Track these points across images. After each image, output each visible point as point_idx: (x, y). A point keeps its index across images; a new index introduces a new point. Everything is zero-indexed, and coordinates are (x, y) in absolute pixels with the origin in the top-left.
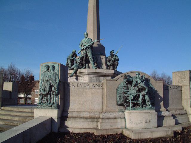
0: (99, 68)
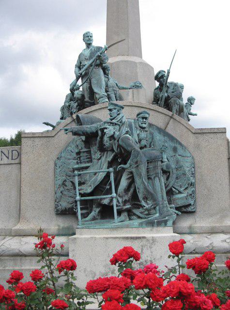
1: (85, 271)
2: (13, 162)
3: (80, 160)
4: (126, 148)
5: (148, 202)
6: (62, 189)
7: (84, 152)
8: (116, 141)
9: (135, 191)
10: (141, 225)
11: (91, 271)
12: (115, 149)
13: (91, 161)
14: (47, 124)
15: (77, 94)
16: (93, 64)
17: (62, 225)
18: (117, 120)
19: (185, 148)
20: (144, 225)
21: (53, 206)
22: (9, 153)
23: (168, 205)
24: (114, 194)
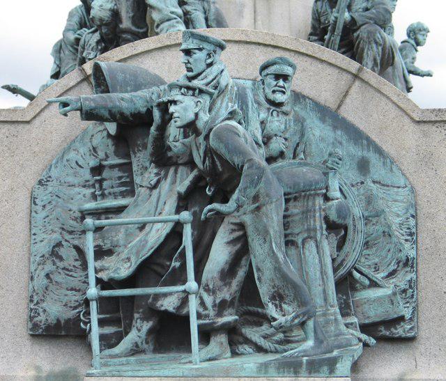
4: (227, 157)
5: (283, 305)
6: (49, 267)
7: (112, 167)
9: (250, 276)
10: (264, 367)
13: (131, 193)
14: (14, 90)
18: (205, 81)
20: (272, 371)
21: (24, 315)
23: (339, 317)
24: (192, 284)
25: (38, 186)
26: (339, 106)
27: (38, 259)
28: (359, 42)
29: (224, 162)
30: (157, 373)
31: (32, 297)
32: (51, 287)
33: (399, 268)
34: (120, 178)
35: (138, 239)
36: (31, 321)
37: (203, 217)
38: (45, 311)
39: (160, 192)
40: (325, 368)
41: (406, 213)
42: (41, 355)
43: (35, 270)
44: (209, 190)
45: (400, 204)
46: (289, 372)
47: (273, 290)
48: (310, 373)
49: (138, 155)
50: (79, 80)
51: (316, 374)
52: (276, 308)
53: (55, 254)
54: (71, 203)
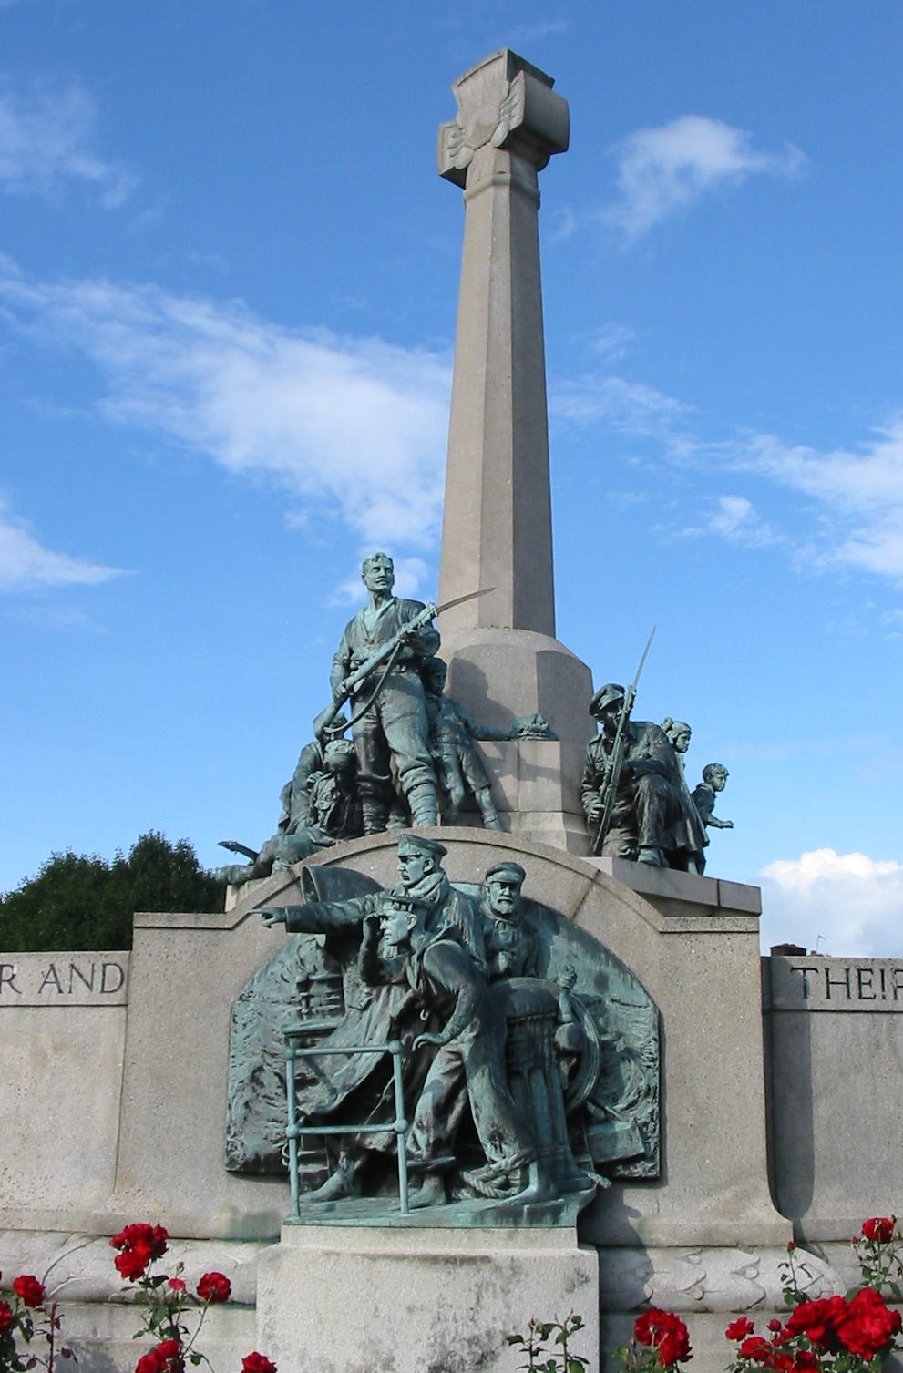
0: (444, 854)
1: (302, 1359)
2: (105, 999)
3: (308, 1004)
4: (442, 981)
5: (504, 1146)
6: (248, 1095)
7: (321, 981)
8: (415, 957)
9: (467, 1108)
10: (480, 1217)
11: (321, 1359)
12: (412, 981)
13: (342, 1011)
14: (235, 847)
15: (335, 752)
16: (391, 658)
17: (244, 1208)
18: (423, 891)
19: (633, 978)
20: (489, 1221)
21: (221, 1150)
22: (93, 971)
23: (570, 1157)
24: (400, 1123)
25: (238, 1002)
26: (575, 915)
27: (236, 1084)
28: (639, 795)
29: (439, 986)
30: (361, 1223)
31: (229, 1127)
32: (250, 1117)
33: (640, 1099)
34: (329, 995)
35: (346, 1067)
36: (228, 1155)
37: (414, 1048)
38: (243, 1144)
39: (371, 1015)
40: (548, 1218)
41: (647, 1036)
42: (238, 1195)
43: (234, 1097)
44: (424, 1015)
45: (642, 1026)
46: (508, 1222)
47: (492, 1129)
48: (531, 1223)
49: (349, 970)
50: (287, 883)
51: (538, 1225)
52: (496, 1148)
53: (255, 1078)
54: (275, 1023)
